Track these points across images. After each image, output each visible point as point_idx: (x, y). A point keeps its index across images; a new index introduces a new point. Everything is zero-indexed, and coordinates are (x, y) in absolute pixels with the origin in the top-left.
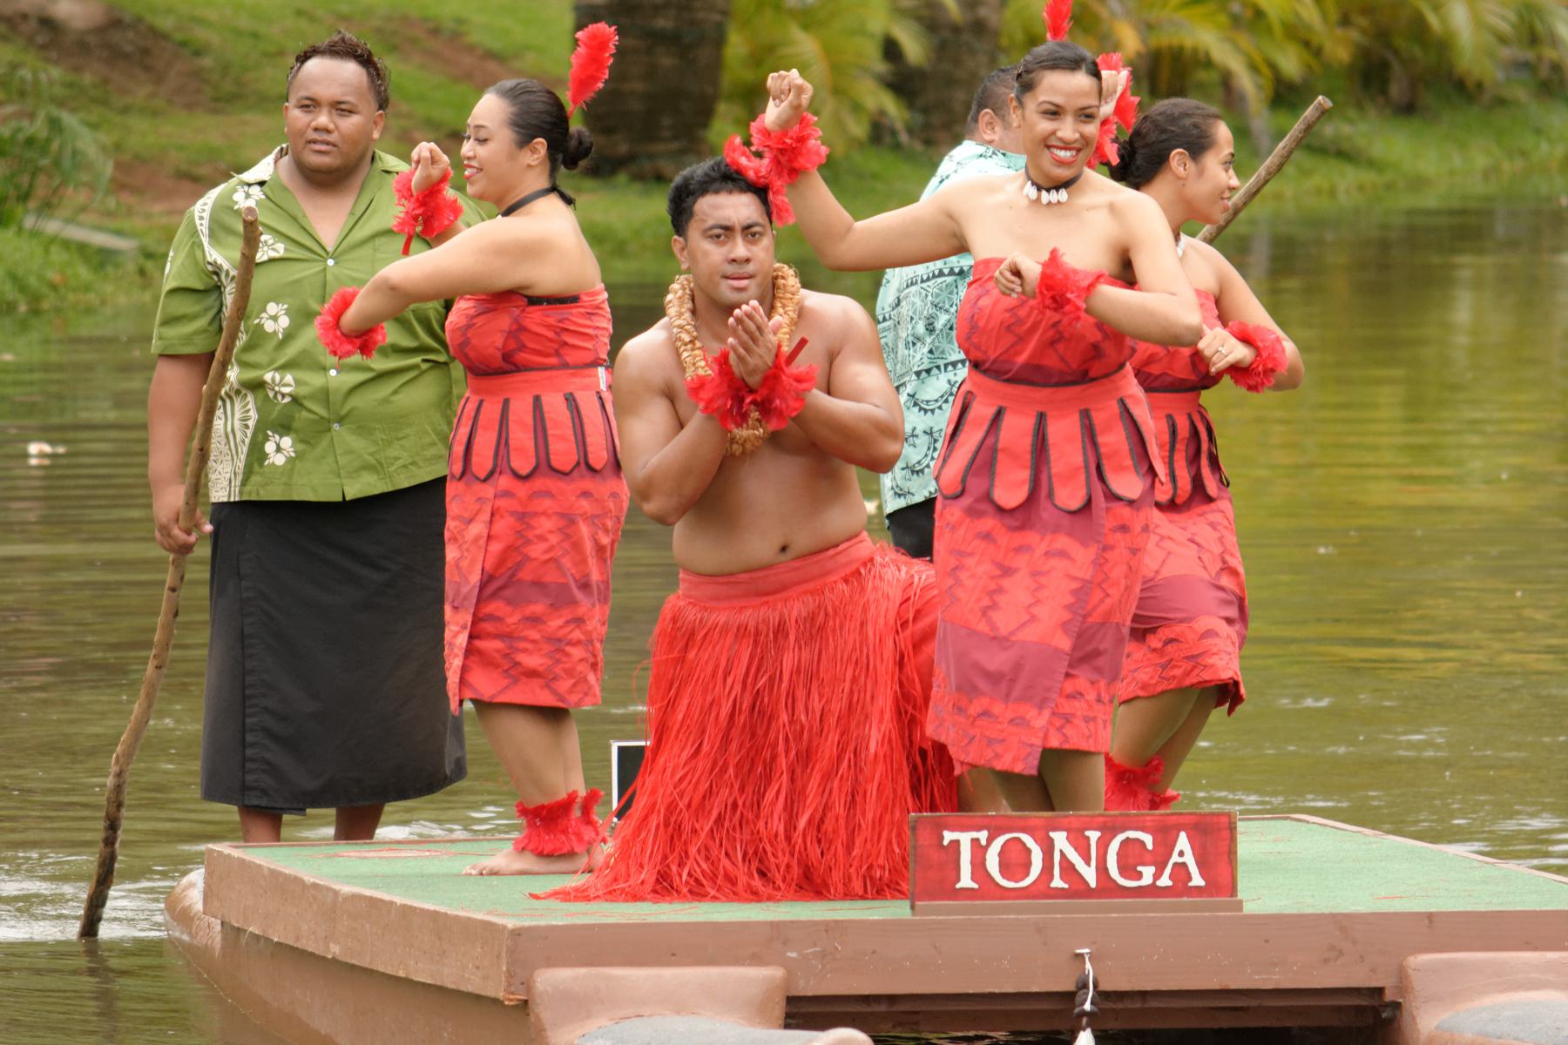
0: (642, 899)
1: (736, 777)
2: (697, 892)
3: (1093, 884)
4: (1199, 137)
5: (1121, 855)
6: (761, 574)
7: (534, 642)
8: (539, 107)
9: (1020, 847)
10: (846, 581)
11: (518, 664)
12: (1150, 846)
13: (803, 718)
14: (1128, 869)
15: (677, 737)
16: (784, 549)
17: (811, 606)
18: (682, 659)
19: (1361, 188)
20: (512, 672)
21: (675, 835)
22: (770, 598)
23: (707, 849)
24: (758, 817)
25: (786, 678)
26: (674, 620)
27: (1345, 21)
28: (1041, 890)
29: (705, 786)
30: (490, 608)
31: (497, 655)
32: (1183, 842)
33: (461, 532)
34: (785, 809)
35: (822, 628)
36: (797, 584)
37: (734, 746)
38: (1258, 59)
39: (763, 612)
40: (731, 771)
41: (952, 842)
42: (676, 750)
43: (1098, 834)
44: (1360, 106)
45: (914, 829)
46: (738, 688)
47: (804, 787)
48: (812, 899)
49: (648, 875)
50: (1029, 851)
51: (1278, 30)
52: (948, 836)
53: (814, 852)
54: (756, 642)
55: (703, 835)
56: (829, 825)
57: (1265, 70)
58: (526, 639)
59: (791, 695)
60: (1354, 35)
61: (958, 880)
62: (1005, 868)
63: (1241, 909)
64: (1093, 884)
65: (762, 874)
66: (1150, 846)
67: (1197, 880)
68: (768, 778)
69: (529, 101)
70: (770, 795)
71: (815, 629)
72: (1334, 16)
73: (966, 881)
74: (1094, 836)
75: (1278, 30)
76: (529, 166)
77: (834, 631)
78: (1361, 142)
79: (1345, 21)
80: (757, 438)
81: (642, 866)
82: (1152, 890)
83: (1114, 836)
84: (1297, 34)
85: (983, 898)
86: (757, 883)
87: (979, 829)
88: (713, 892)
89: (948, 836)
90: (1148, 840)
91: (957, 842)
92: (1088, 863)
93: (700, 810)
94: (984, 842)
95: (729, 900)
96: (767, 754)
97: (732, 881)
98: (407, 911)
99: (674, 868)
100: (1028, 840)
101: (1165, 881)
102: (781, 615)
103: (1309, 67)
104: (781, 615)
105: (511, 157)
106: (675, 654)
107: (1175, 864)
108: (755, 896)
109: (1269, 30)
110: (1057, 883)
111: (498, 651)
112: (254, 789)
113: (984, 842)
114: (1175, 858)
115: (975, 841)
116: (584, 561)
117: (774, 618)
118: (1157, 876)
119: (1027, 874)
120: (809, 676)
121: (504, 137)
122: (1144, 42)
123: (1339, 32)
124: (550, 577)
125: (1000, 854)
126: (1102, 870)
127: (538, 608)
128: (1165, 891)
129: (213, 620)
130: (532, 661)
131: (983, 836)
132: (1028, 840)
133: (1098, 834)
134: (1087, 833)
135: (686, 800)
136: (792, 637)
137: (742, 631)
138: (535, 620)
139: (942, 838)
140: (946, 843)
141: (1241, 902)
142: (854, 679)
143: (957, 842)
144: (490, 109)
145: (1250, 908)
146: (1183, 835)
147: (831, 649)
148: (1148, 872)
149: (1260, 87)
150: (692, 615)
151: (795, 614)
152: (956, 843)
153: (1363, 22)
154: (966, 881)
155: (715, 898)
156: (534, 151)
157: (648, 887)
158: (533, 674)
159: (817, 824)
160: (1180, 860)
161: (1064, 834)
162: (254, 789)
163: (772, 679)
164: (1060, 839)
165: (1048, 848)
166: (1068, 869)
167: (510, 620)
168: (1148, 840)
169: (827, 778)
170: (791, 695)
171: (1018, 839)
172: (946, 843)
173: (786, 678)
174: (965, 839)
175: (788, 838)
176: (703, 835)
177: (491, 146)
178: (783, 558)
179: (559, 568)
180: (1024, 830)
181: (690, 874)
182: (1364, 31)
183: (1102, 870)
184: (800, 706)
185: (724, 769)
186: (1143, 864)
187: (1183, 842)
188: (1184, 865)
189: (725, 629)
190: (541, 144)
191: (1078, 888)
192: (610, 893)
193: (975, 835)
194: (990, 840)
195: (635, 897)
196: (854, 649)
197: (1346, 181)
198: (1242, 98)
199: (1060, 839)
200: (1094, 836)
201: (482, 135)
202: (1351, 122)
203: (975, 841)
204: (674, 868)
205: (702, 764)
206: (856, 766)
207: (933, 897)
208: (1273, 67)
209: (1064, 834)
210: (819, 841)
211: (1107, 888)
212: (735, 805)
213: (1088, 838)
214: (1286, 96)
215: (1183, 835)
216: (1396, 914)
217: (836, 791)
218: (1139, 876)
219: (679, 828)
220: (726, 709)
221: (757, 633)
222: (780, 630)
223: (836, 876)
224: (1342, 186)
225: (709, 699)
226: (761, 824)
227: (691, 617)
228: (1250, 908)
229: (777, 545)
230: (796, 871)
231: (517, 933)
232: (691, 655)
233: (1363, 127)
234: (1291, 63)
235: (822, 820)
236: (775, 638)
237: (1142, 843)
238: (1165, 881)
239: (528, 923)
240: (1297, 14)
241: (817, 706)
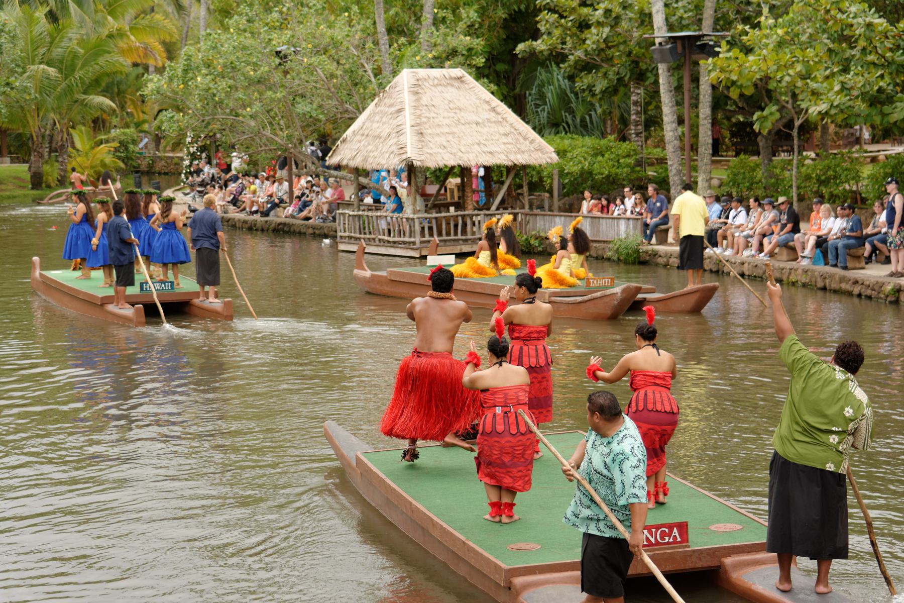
4: (656, 117)
14: (662, 538)
32: (675, 530)
67: (679, 539)
71: (541, 207)
74: (654, 530)
82: (668, 543)
90: (667, 530)
126: (656, 539)
128: (671, 543)
129: (770, 511)
148: (667, 538)
168: (667, 530)
183: (656, 539)
187: (675, 530)
200: (654, 530)
211: (657, 543)
238: (671, 540)
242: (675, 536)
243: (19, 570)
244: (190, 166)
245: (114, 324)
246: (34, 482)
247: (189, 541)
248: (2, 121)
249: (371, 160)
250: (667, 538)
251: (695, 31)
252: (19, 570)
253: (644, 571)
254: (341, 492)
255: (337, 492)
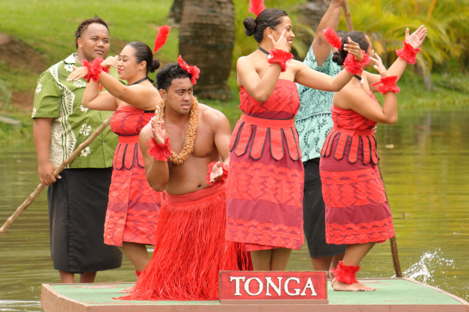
0: (147, 299)
1: (181, 260)
2: (166, 297)
3: (280, 295)
5: (289, 285)
6: (192, 194)
7: (143, 223)
8: (145, 51)
9: (256, 282)
10: (220, 196)
11: (138, 230)
12: (299, 282)
13: (204, 241)
15: (162, 247)
16: (199, 186)
17: (208, 204)
18: (166, 222)
19: (464, 101)
20: (136, 233)
21: (160, 278)
22: (195, 202)
23: (170, 283)
24: (187, 273)
25: (199, 228)
26: (165, 209)
27: (458, 41)
28: (263, 296)
29: (171, 262)
30: (130, 211)
31: (132, 227)
32: (309, 281)
33: (120, 187)
34: (196, 271)
35: (212, 211)
36: (204, 197)
37: (180, 250)
38: (426, 55)
39: (193, 206)
40: (179, 258)
41: (233, 280)
42: (162, 251)
43: (282, 278)
44: (463, 72)
45: (221, 276)
46: (183, 231)
47: (203, 263)
48: (203, 300)
49: (150, 291)
50: (259, 283)
51: (433, 44)
52: (232, 278)
53: (205, 284)
54: (190, 216)
55: (169, 278)
56: (209, 276)
57: (429, 59)
58: (141, 222)
59: (201, 233)
60: (461, 46)
61: (235, 293)
62: (250, 289)
63: (328, 303)
64: (280, 295)
65: (187, 292)
66: (299, 282)
67: (314, 294)
68: (191, 260)
69: (141, 49)
70: (192, 265)
72: (454, 39)
73: (238, 293)
74: (280, 279)
75: (433, 44)
76: (140, 70)
77: (215, 212)
78: (464, 85)
79: (458, 41)
80: (42, 88)
81: (149, 288)
82: (299, 297)
83: (287, 279)
84: (441, 46)
85: (243, 299)
86: (186, 294)
87: (242, 276)
88: (172, 298)
89: (232, 278)
90: (298, 280)
91: (235, 280)
92: (278, 288)
93: (169, 270)
94: (244, 280)
95: (176, 300)
96: (191, 253)
97: (177, 293)
98: (68, 301)
99: (159, 289)
100: (258, 279)
101: (303, 294)
102: (199, 207)
103: (445, 58)
104: (199, 207)
105: (135, 67)
106: (164, 220)
107: (307, 288)
108: (184, 298)
109: (430, 45)
110: (268, 294)
111: (132, 226)
112: (71, 266)
113: (244, 280)
114: (307, 286)
115: (241, 280)
116: (160, 197)
117: (196, 208)
118: (301, 292)
119: (258, 291)
120: (208, 227)
121: (132, 60)
122: (385, 49)
123: (456, 45)
124: (150, 201)
125: (249, 284)
126: (283, 290)
127: (145, 212)
130: (143, 229)
131: (243, 278)
132: (258, 279)
133: (282, 278)
134: (278, 278)
135: (164, 267)
136: (202, 215)
137: (186, 213)
138: (144, 216)
139: (230, 279)
140: (231, 280)
141: (328, 301)
142: (221, 228)
143: (235, 280)
144: (128, 50)
145: (330, 303)
146: (309, 279)
147: (214, 218)
148: (298, 291)
149: (427, 65)
150: (170, 208)
151: (203, 207)
152: (234, 281)
153: (465, 42)
154: (238, 293)
155: (172, 299)
156: (142, 65)
157: (150, 296)
158: (143, 233)
159: (206, 275)
160: (309, 287)
161: (270, 278)
162: (71, 266)
163: (194, 227)
164: (269, 280)
165: (265, 283)
166: (271, 289)
167: (136, 216)
168: (298, 280)
169: (210, 260)
170: (201, 233)
171: (255, 279)
172: (231, 280)
173: (199, 228)
174: (238, 279)
175: (196, 280)
176: (169, 278)
177: (128, 62)
178: (199, 189)
179: (153, 198)
180: (257, 277)
181: (164, 291)
182: (464, 45)
183: (283, 290)
184: (203, 237)
185: (177, 258)
186: (297, 288)
187: (309, 281)
188: (310, 288)
189: (180, 212)
190: (144, 63)
191: (275, 296)
192: (138, 297)
193: (241, 278)
194: (246, 280)
195: (145, 299)
196: (221, 218)
197: (458, 100)
198: (421, 69)
199: (269, 280)
200: (280, 279)
201: (125, 59)
202: (461, 78)
203: (241, 280)
204: (159, 289)
205: (170, 256)
206: (220, 257)
207: (227, 298)
208: (432, 58)
209: (270, 278)
210: (206, 281)
211: (284, 296)
212: (180, 269)
213: (278, 279)
214: (436, 68)
215: (309, 279)
216: (379, 305)
217: (213, 264)
218: (295, 292)
219: (161, 275)
220: (179, 238)
221: (191, 213)
222: (198, 212)
223: (211, 292)
224: (457, 102)
225: (174, 235)
226: (188, 274)
227: (170, 208)
228: (330, 303)
229: (197, 184)
230: (199, 290)
231: (88, 308)
232: (169, 220)
233: (465, 80)
234: (439, 57)
235: (208, 274)
236: (197, 215)
237: (296, 281)
238: (303, 294)
239: (92, 305)
240: (441, 39)
241: (208, 236)
242: (309, 289)
245: (250, 153)
246: (17, 243)
247: (151, 245)
249: (300, 182)
253: (95, 280)
255: (401, 151)
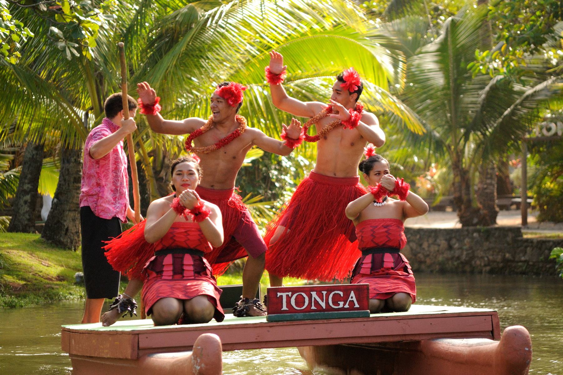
14: (335, 303)
32: (352, 294)
50: (304, 298)
67: (357, 306)
74: (324, 293)
82: (343, 309)
90: (342, 294)
114: (350, 299)
126: (327, 303)
128: (347, 309)
148: (341, 304)
168: (342, 294)
183: (327, 303)
187: (352, 294)
200: (324, 293)
211: (329, 308)
238: (347, 306)
242: (352, 302)
243: (276, 31)
244: (146, 31)
248: (562, 106)
250: (341, 304)
251: (78, 237)
252: (276, 31)
254: (41, 206)
